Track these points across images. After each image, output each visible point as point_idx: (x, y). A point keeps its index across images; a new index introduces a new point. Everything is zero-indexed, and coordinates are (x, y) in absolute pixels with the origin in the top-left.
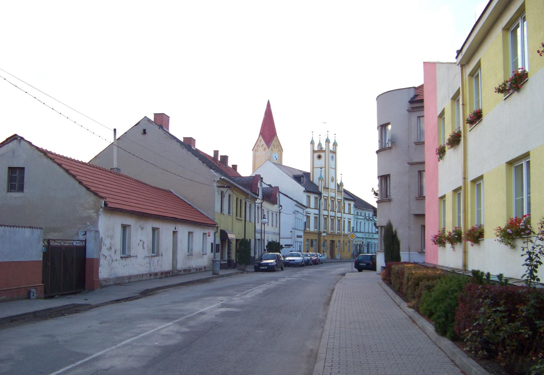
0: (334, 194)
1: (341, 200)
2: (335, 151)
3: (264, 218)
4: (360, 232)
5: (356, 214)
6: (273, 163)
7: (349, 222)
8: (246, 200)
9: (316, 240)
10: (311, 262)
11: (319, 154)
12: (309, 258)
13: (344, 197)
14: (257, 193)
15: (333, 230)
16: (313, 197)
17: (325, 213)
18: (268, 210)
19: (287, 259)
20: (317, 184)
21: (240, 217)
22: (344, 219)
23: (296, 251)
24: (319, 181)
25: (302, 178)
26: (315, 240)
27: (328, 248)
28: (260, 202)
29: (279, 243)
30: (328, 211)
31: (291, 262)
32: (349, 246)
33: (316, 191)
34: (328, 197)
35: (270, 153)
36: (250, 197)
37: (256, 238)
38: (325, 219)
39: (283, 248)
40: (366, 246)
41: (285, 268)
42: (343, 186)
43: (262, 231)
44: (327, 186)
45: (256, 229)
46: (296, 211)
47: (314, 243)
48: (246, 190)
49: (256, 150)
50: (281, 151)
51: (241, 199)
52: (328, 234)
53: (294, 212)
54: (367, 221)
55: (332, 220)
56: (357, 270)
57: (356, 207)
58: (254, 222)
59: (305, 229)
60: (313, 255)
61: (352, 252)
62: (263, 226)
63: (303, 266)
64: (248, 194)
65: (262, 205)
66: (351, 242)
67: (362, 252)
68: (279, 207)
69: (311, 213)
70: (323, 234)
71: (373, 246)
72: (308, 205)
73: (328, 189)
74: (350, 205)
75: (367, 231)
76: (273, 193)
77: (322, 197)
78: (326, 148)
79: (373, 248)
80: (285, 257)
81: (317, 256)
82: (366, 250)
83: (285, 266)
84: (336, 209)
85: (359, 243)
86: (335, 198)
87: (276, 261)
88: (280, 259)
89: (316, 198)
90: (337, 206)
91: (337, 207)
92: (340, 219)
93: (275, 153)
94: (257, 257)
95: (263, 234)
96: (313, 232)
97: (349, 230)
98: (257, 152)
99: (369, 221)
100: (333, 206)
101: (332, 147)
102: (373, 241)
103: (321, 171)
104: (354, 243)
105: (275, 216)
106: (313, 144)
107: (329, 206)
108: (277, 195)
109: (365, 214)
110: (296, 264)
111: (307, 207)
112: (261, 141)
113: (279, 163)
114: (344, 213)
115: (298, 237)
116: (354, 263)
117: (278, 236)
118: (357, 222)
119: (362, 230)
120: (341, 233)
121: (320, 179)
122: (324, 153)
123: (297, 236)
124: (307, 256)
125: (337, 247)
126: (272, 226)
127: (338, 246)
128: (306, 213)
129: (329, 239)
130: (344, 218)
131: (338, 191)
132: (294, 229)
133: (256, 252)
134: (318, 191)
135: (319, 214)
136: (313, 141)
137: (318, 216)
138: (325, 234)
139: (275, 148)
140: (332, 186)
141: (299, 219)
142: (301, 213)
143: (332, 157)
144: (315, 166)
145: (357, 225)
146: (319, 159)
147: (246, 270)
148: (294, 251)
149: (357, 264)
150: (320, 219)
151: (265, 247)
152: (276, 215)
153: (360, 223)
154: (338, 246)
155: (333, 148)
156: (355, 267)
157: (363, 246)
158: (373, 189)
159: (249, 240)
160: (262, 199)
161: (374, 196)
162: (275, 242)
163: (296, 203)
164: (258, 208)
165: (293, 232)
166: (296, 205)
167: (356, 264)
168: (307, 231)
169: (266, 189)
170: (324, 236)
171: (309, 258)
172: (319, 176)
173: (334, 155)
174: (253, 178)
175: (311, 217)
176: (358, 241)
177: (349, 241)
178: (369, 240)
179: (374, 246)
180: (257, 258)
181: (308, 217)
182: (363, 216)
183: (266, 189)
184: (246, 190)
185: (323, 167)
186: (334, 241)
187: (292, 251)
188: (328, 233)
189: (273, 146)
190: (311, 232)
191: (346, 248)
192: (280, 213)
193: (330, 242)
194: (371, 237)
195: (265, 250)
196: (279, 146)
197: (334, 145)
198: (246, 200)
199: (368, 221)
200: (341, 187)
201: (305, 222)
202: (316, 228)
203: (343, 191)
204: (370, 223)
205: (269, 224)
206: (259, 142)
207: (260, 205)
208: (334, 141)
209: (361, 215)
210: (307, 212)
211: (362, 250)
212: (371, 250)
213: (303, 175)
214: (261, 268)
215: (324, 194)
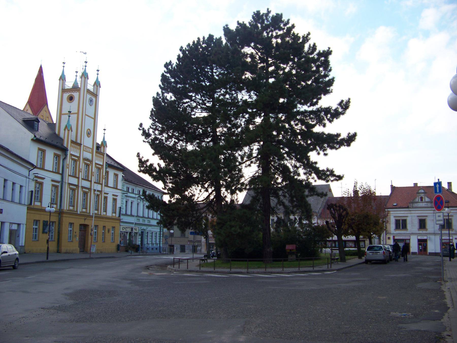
0: (91, 155)
1: (102, 166)
4: (131, 215)
7: (115, 200)
11: (70, 94)
13: (106, 163)
15: (98, 210)
16: (50, 153)
17: (74, 181)
27: (76, 236)
33: (59, 145)
34: (79, 157)
55: (85, 194)
57: (125, 180)
69: (45, 178)
71: (149, 235)
73: (80, 145)
74: (116, 175)
75: (141, 215)
79: (149, 237)
82: (140, 240)
86: (91, 161)
89: (57, 156)
97: (114, 211)
102: (149, 228)
104: (121, 230)
106: (63, 80)
107: (79, 171)
111: (35, 167)
114: (107, 186)
118: (126, 202)
122: (78, 93)
128: (36, 177)
129: (78, 222)
131: (96, 152)
134: (62, 145)
135: (62, 181)
136: (64, 76)
137: (59, 184)
140: (87, 142)
143: (91, 101)
145: (126, 206)
146: (69, 101)
153: (132, 203)
158: (141, 125)
161: (143, 137)
173: (94, 99)
176: (127, 228)
178: (144, 227)
179: (151, 235)
182: (136, 194)
186: (89, 225)
191: (109, 237)
194: (146, 222)
199: (143, 201)
201: (32, 191)
208: (95, 80)
210: (36, 175)
212: (146, 240)
215: (72, 151)
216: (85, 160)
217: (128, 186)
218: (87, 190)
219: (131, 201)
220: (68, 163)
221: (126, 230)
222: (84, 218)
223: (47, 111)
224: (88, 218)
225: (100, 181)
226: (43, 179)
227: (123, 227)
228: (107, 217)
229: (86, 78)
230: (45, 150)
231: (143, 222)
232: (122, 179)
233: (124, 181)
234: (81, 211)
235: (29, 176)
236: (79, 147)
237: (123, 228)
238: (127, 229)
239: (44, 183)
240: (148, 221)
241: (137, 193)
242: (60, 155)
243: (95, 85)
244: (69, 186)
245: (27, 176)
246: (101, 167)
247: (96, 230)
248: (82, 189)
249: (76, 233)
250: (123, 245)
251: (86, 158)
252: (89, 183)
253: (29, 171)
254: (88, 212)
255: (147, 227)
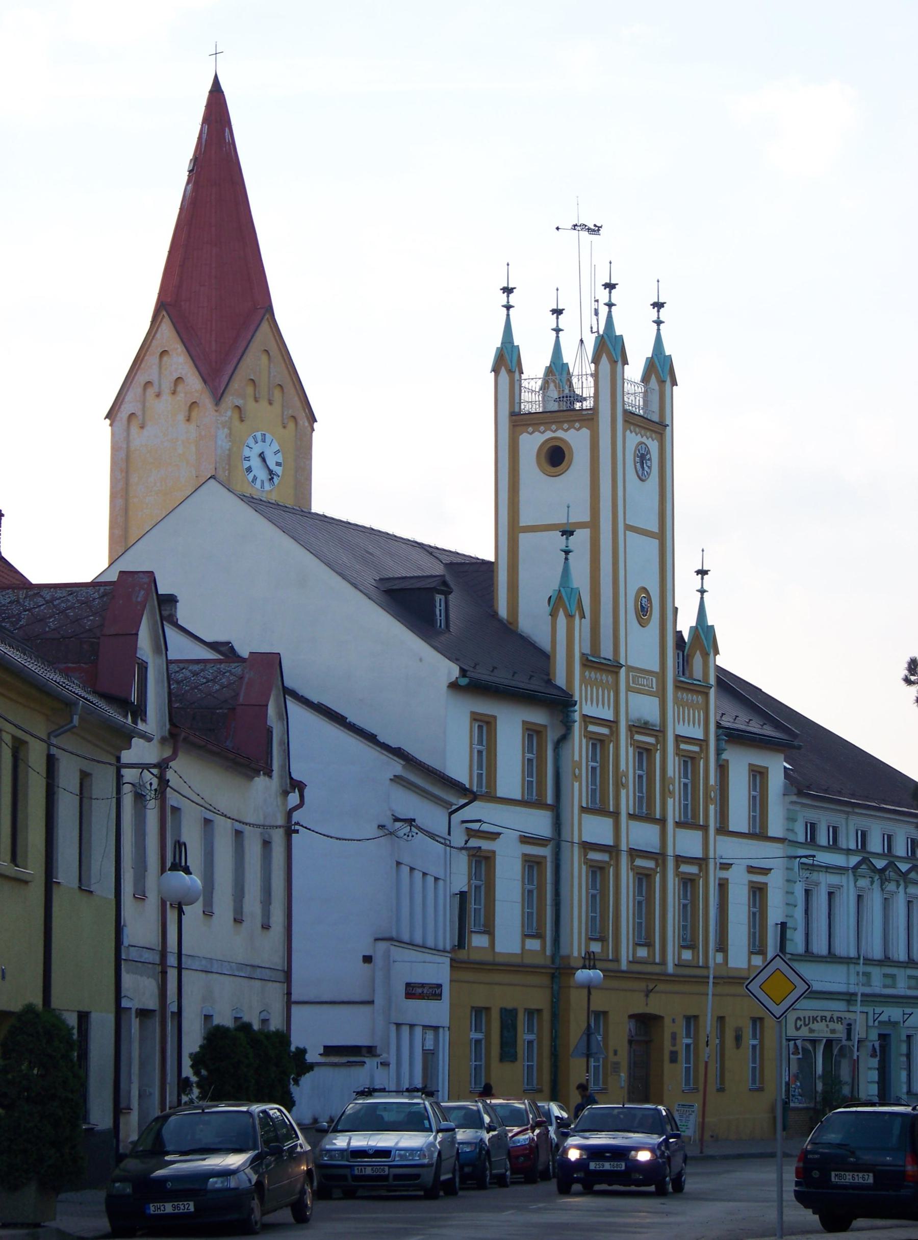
0: (656, 701)
1: (702, 743)
2: (656, 418)
3: (175, 867)
4: (832, 958)
5: (801, 839)
6: (243, 498)
7: (758, 892)
8: (54, 741)
9: (539, 1011)
10: (502, 1165)
11: (549, 435)
12: (487, 1136)
13: (719, 726)
14: (134, 697)
18: (210, 815)
19: (341, 1142)
20: (542, 639)
21: (14, 859)
22: (724, 874)
23: (399, 1092)
24: (553, 614)
25: (439, 598)
26: (530, 1013)
27: (616, 1067)
28: (154, 760)
29: (283, 1038)
30: (616, 815)
31: (367, 1168)
32: (758, 1052)
33: (536, 685)
34: (612, 725)
35: (230, 435)
36: (81, 719)
37: (125, 1003)
38: (597, 871)
39: (311, 1067)
40: (873, 1055)
41: (323, 1204)
42: (717, 652)
43: (163, 954)
44: (606, 651)
45: (126, 942)
46: (397, 820)
47: (524, 1036)
48: (52, 677)
49: (132, 415)
50: (303, 422)
51: (19, 734)
52: (612, 974)
53: (388, 822)
54: (898, 886)
55: (643, 878)
56: (810, 1217)
57: (800, 793)
58: (112, 896)
59: (461, 943)
60: (517, 1117)
61: (774, 1090)
62: (172, 916)
63: (449, 1189)
64: (69, 705)
65: (170, 775)
66: (770, 1022)
67: (846, 1090)
68: (286, 793)
69: (499, 834)
70: (582, 975)
72: (480, 776)
73: (613, 667)
74: (758, 775)
75: (878, 954)
76: (241, 699)
77: (577, 726)
78: (596, 396)
80: (325, 1131)
81: (538, 1124)
82: (874, 1075)
83: (322, 1194)
84: (670, 801)
85: (822, 1031)
86: (659, 732)
87: (255, 1163)
88: (287, 1145)
89: (533, 733)
90: (676, 788)
91: (672, 794)
92: (693, 869)
93: (259, 435)
94: (131, 1130)
95: (172, 974)
96: (518, 960)
97: (757, 947)
98: (142, 427)
99: (889, 880)
100: (646, 780)
101: (640, 389)
103: (567, 552)
104: (792, 1032)
105: (253, 849)
106: (510, 372)
107: (618, 785)
108: (271, 711)
109: (864, 835)
110: (397, 1177)
111: (471, 796)
112: (164, 353)
113: (289, 503)
114: (723, 830)
115: (413, 991)
116: (792, 1169)
117: (276, 991)
118: (807, 892)
119: (845, 946)
120: (706, 967)
121: (557, 603)
122: (585, 432)
123: (408, 985)
124: (473, 1120)
125: (674, 1058)
126: (238, 921)
127: (682, 1056)
128: (471, 834)
130: (726, 866)
131: (679, 686)
132: (391, 939)
133: (123, 1093)
134: (549, 682)
135: (557, 840)
137: (545, 852)
138: (595, 974)
139: (264, 403)
141: (418, 875)
142: (432, 836)
143: (642, 458)
144: (525, 520)
147: (53, 1224)
148: (383, 1090)
149: (816, 1174)
150: (564, 874)
151: (187, 1062)
152: (267, 844)
153: (830, 894)
154: (682, 1056)
155: (646, 394)
156: (800, 1197)
157: (852, 1051)
159: (72, 1020)
160: (163, 741)
162: (256, 1027)
163: (397, 767)
164: (139, 797)
165: (378, 960)
166: (397, 779)
167: (803, 1175)
168: (475, 956)
169: (196, 668)
170: (589, 988)
171: (487, 1136)
172: (553, 584)
173: (653, 446)
174: (105, 594)
175: (499, 861)
176: (815, 1019)
177: (757, 1021)
178: (894, 1013)
180: (134, 1137)
181: (478, 863)
182: (848, 852)
183: (196, 668)
184: (52, 677)
185: (582, 525)
187: (369, 1092)
188: (611, 966)
189: (250, 390)
190: (499, 960)
192: (290, 831)
193: (632, 1024)
195: (184, 1085)
196: (290, 390)
197: (653, 379)
198: (54, 741)
200: (697, 660)
201: (463, 895)
202: (532, 931)
203: (712, 681)
204: (892, 894)
205: (216, 909)
206: (152, 359)
207: (155, 781)
209: (834, 846)
210: (475, 826)
211: (845, 1073)
212: (904, 1074)
213: (448, 578)
214: (152, 1209)
216: (638, 733)
217: (812, 815)
218: (650, 864)
219: (830, 886)
220: (577, 758)
221: (811, 1031)
222: (642, 985)
223: (274, 351)
224: (661, 987)
225: (695, 814)
226: (494, 839)
227: (799, 1018)
228: (732, 974)
229: (616, 362)
230: (495, 718)
231: (885, 986)
232: (785, 787)
233: (794, 798)
234: (631, 959)
235: (449, 834)
236: (610, 679)
237: (799, 1023)
238: (815, 1026)
239: (497, 853)
240: (910, 977)
241: (852, 846)
242: (545, 726)
243: (653, 378)
244: (585, 856)
245: (443, 831)
246: (696, 749)
247: (688, 1036)
248: (633, 861)
249: (615, 1053)
250: (797, 1105)
251: (639, 720)
252: (655, 829)
253: (451, 814)
254: (657, 960)
255: (908, 1011)
